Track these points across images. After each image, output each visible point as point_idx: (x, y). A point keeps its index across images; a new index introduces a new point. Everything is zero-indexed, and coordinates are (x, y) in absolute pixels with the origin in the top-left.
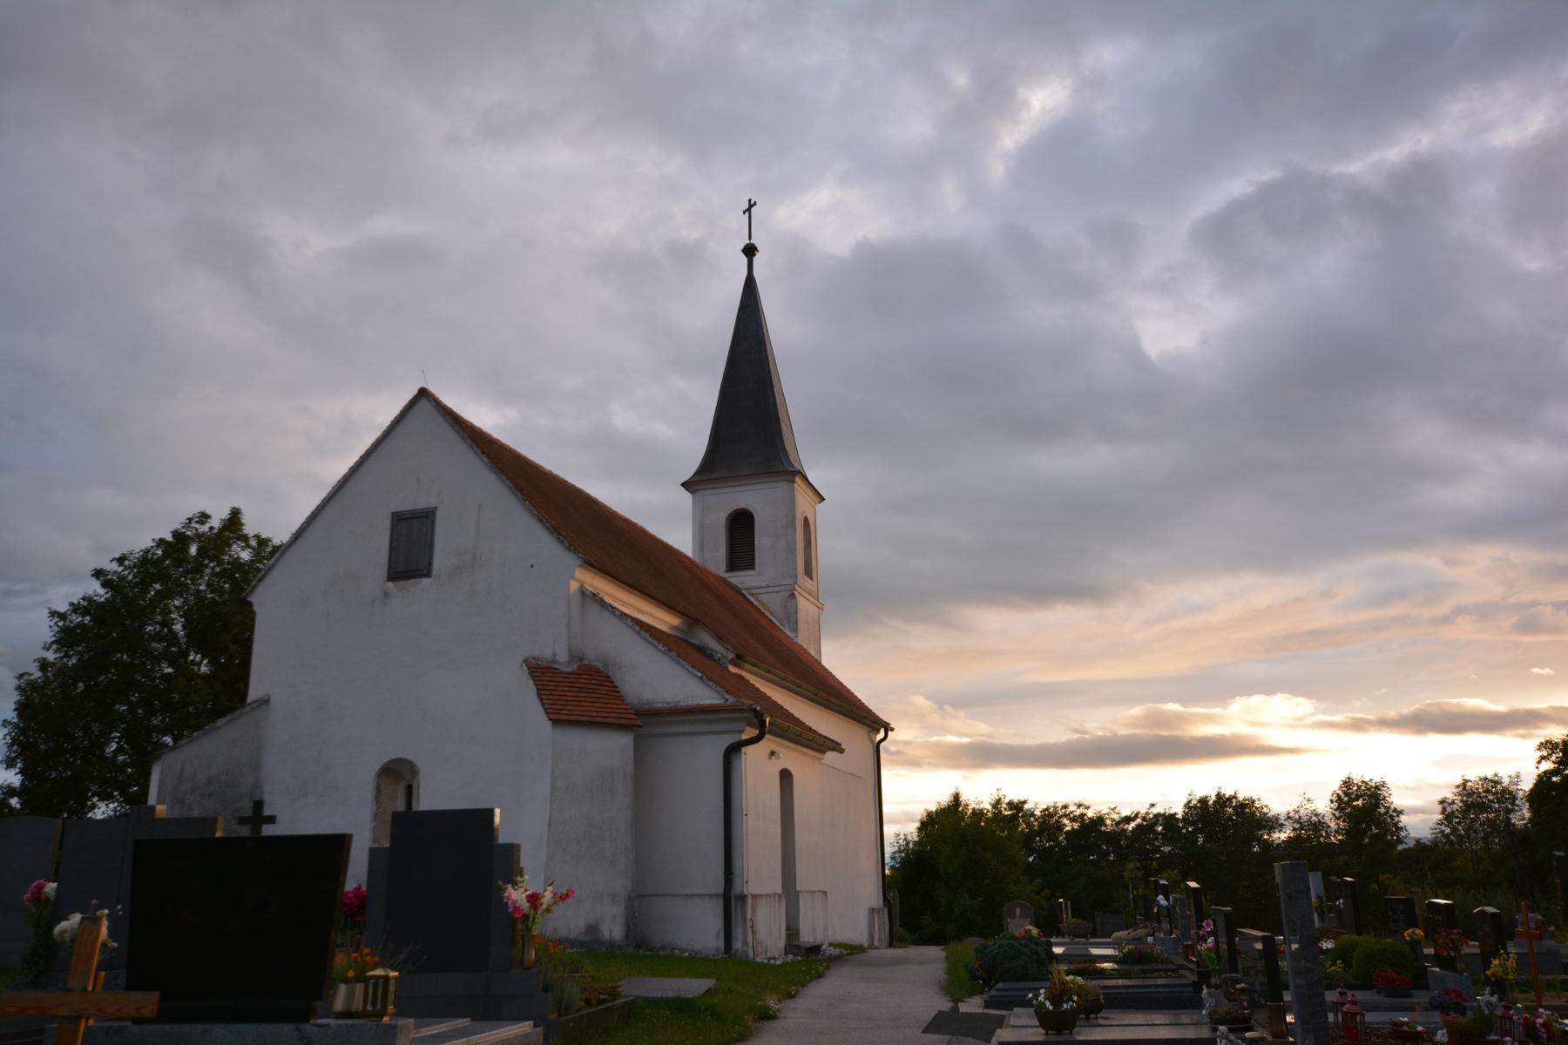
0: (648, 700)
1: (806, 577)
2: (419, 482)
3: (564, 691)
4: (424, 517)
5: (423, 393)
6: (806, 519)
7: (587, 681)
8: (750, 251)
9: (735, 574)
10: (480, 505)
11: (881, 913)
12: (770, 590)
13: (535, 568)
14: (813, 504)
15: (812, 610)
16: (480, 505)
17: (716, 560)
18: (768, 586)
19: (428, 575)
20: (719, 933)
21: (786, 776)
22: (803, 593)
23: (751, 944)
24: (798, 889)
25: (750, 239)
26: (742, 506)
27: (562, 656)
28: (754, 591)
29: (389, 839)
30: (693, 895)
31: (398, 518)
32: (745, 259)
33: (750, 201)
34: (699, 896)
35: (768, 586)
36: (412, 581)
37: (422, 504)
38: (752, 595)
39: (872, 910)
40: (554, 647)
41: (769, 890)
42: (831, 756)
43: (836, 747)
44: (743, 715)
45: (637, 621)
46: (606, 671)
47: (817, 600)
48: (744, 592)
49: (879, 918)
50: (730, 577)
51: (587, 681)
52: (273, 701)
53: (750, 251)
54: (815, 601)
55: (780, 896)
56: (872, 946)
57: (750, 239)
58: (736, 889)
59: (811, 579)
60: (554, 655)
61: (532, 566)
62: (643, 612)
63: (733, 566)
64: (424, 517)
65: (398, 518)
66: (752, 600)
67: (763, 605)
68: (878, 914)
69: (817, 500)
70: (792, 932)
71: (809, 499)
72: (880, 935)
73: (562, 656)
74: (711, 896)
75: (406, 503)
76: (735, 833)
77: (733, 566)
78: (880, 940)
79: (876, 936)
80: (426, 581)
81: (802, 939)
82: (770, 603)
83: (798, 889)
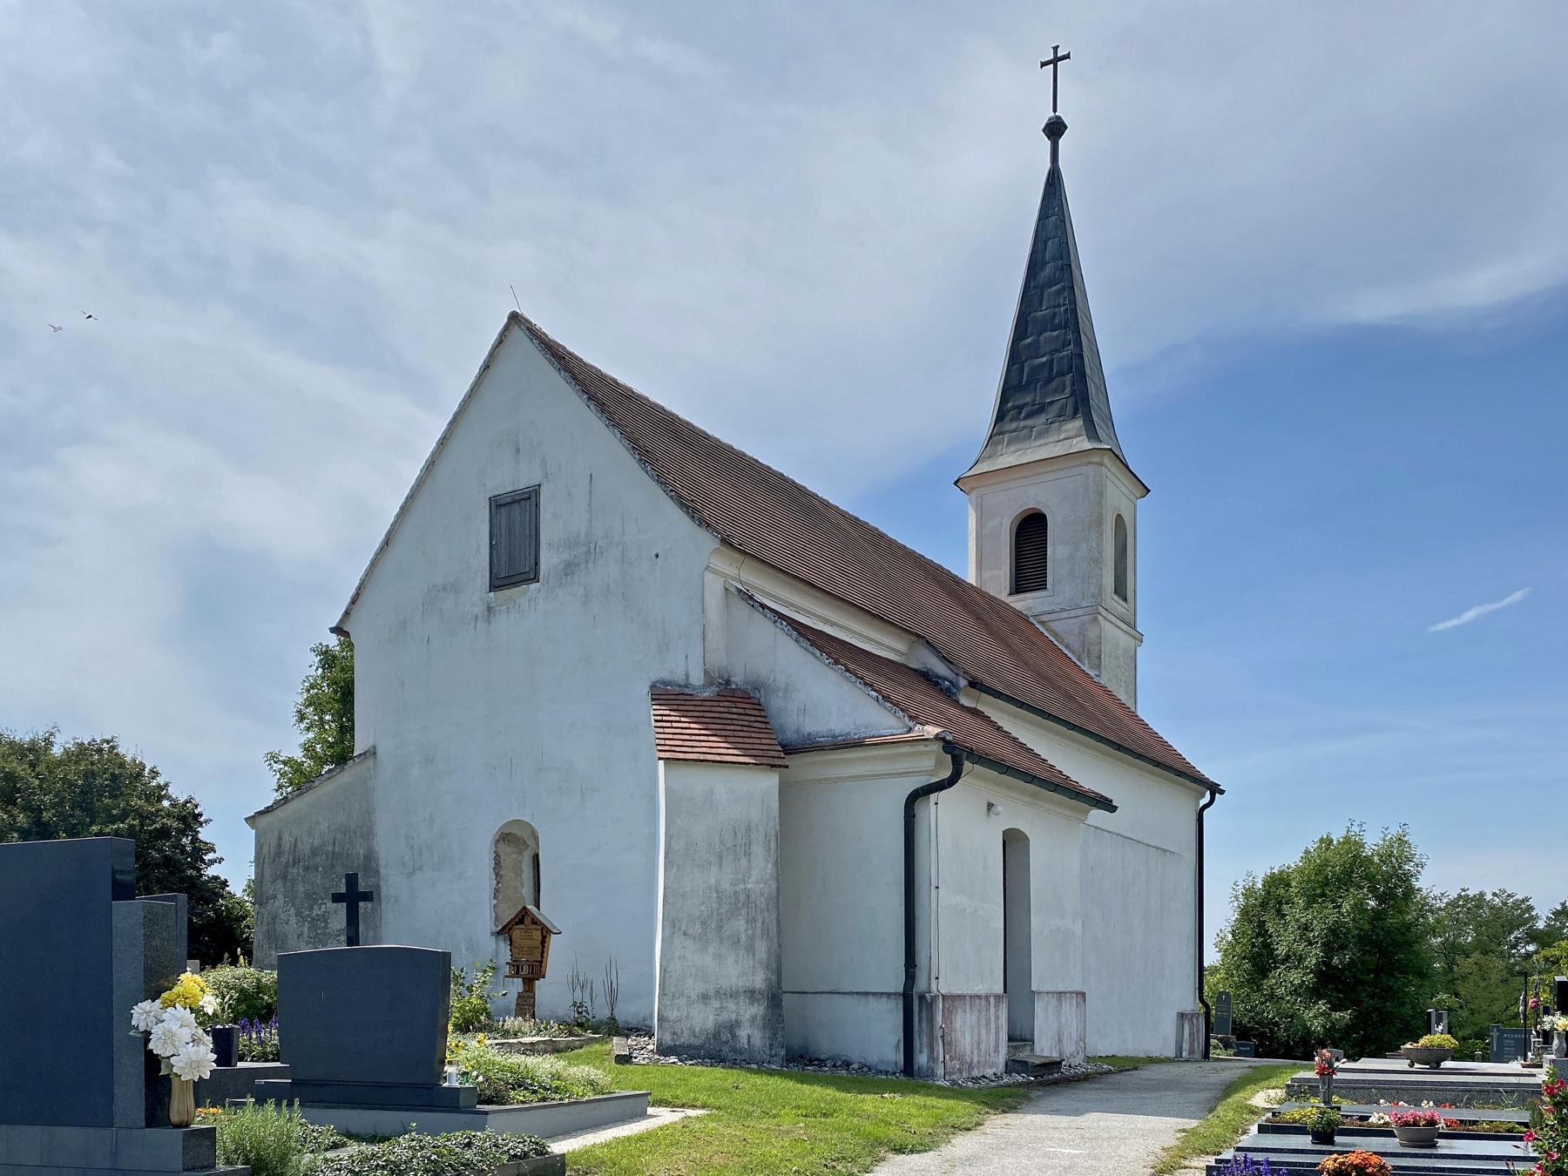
0: (809, 734)
1: (1116, 597)
2: (518, 451)
3: (671, 722)
4: (525, 499)
5: (515, 318)
6: (1119, 517)
7: (726, 710)
8: (1055, 129)
9: (1022, 596)
10: (591, 476)
11: (1194, 1020)
12: (1065, 615)
13: (655, 558)
14: (1132, 498)
15: (1124, 640)
16: (591, 476)
17: (998, 583)
18: (1063, 610)
19: (536, 579)
20: (898, 1045)
21: (1013, 843)
22: (1111, 617)
23: (941, 1059)
24: (1034, 988)
25: (1055, 111)
26: (1031, 505)
27: (697, 678)
28: (1045, 618)
29: (361, 911)
30: (867, 994)
31: (498, 505)
32: (1047, 143)
33: (1056, 49)
34: (874, 994)
35: (1063, 610)
36: (514, 591)
37: (524, 481)
38: (1043, 623)
39: (1182, 1016)
40: (688, 668)
41: (980, 988)
42: (1097, 816)
43: (1107, 805)
44: (928, 749)
45: (792, 623)
46: (757, 695)
47: (1134, 628)
48: (1032, 620)
49: (1191, 1028)
50: (1012, 602)
51: (726, 710)
52: (379, 751)
53: (1055, 129)
54: (1132, 631)
55: (997, 997)
56: (1177, 1059)
57: (1055, 111)
58: (921, 985)
59: (1125, 600)
60: (687, 676)
61: (657, 556)
62: (832, 624)
63: (1019, 587)
64: (525, 499)
65: (498, 505)
66: (1042, 629)
67: (1056, 635)
68: (1191, 1019)
69: (1138, 491)
70: (1019, 1037)
71: (1123, 489)
72: (1192, 1044)
73: (697, 678)
74: (889, 995)
75: (506, 480)
76: (920, 912)
77: (1019, 587)
78: (1191, 1051)
79: (1186, 1046)
80: (533, 586)
81: (1038, 1051)
82: (1064, 630)
83: (1034, 988)
